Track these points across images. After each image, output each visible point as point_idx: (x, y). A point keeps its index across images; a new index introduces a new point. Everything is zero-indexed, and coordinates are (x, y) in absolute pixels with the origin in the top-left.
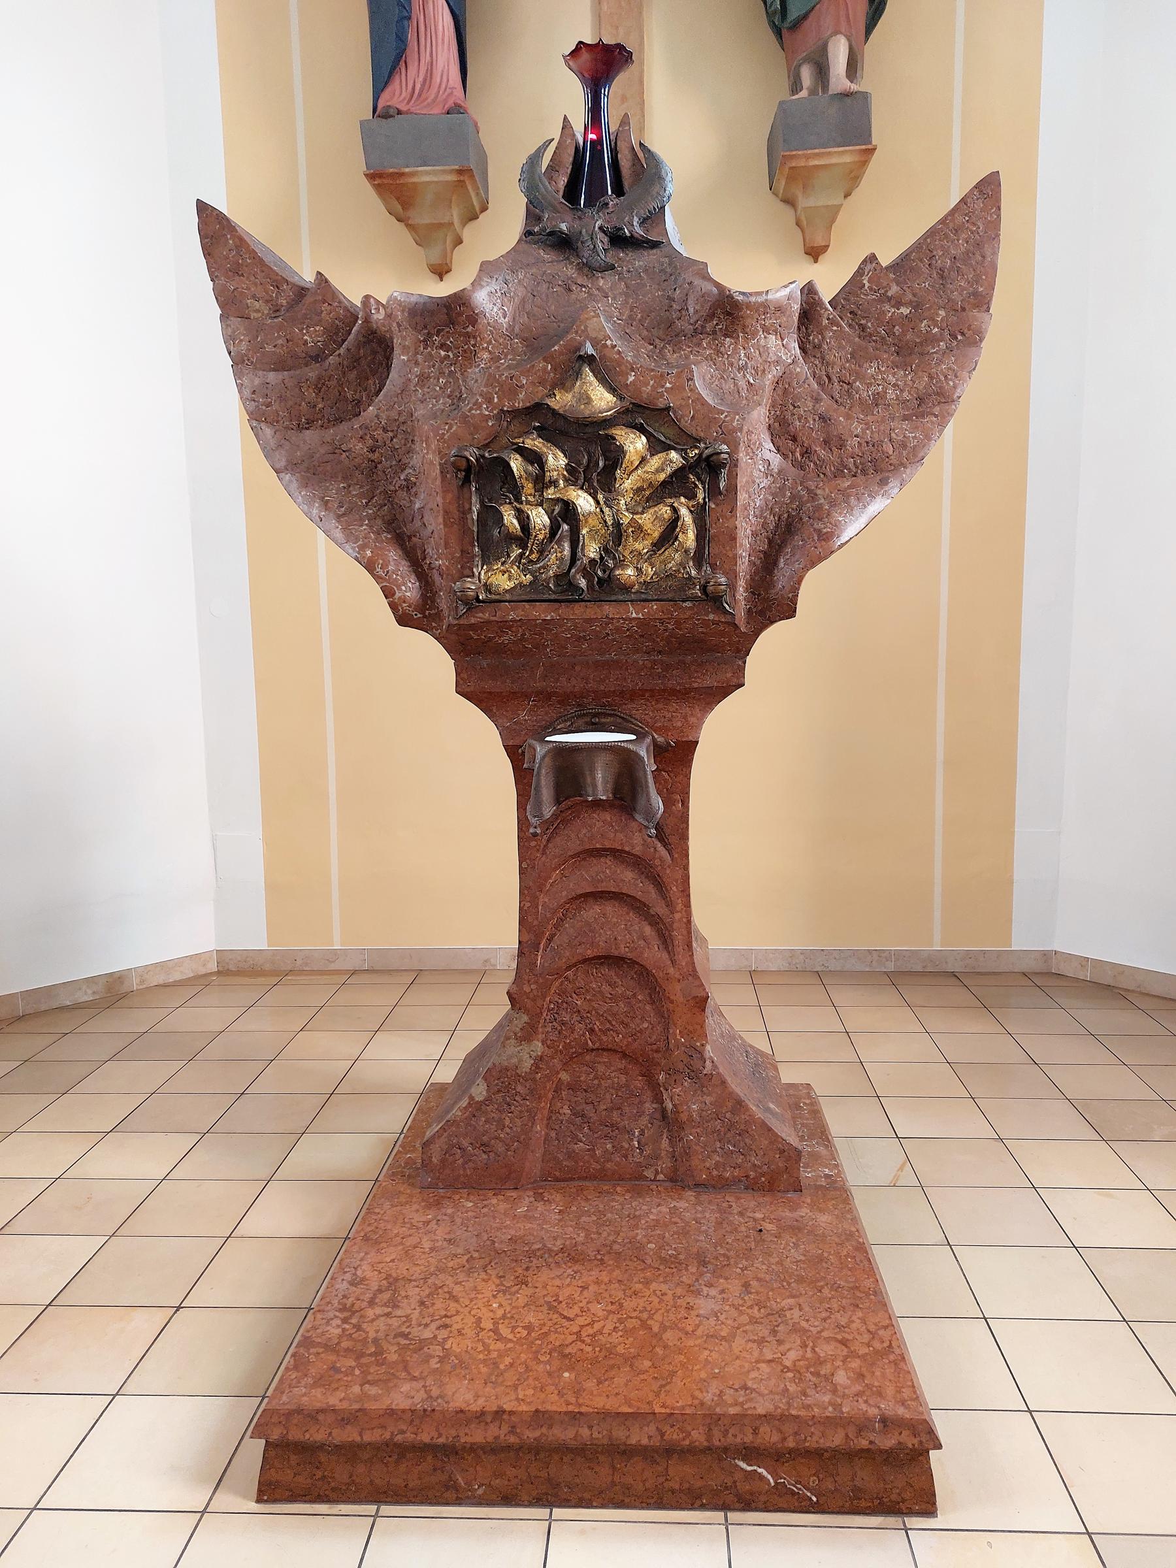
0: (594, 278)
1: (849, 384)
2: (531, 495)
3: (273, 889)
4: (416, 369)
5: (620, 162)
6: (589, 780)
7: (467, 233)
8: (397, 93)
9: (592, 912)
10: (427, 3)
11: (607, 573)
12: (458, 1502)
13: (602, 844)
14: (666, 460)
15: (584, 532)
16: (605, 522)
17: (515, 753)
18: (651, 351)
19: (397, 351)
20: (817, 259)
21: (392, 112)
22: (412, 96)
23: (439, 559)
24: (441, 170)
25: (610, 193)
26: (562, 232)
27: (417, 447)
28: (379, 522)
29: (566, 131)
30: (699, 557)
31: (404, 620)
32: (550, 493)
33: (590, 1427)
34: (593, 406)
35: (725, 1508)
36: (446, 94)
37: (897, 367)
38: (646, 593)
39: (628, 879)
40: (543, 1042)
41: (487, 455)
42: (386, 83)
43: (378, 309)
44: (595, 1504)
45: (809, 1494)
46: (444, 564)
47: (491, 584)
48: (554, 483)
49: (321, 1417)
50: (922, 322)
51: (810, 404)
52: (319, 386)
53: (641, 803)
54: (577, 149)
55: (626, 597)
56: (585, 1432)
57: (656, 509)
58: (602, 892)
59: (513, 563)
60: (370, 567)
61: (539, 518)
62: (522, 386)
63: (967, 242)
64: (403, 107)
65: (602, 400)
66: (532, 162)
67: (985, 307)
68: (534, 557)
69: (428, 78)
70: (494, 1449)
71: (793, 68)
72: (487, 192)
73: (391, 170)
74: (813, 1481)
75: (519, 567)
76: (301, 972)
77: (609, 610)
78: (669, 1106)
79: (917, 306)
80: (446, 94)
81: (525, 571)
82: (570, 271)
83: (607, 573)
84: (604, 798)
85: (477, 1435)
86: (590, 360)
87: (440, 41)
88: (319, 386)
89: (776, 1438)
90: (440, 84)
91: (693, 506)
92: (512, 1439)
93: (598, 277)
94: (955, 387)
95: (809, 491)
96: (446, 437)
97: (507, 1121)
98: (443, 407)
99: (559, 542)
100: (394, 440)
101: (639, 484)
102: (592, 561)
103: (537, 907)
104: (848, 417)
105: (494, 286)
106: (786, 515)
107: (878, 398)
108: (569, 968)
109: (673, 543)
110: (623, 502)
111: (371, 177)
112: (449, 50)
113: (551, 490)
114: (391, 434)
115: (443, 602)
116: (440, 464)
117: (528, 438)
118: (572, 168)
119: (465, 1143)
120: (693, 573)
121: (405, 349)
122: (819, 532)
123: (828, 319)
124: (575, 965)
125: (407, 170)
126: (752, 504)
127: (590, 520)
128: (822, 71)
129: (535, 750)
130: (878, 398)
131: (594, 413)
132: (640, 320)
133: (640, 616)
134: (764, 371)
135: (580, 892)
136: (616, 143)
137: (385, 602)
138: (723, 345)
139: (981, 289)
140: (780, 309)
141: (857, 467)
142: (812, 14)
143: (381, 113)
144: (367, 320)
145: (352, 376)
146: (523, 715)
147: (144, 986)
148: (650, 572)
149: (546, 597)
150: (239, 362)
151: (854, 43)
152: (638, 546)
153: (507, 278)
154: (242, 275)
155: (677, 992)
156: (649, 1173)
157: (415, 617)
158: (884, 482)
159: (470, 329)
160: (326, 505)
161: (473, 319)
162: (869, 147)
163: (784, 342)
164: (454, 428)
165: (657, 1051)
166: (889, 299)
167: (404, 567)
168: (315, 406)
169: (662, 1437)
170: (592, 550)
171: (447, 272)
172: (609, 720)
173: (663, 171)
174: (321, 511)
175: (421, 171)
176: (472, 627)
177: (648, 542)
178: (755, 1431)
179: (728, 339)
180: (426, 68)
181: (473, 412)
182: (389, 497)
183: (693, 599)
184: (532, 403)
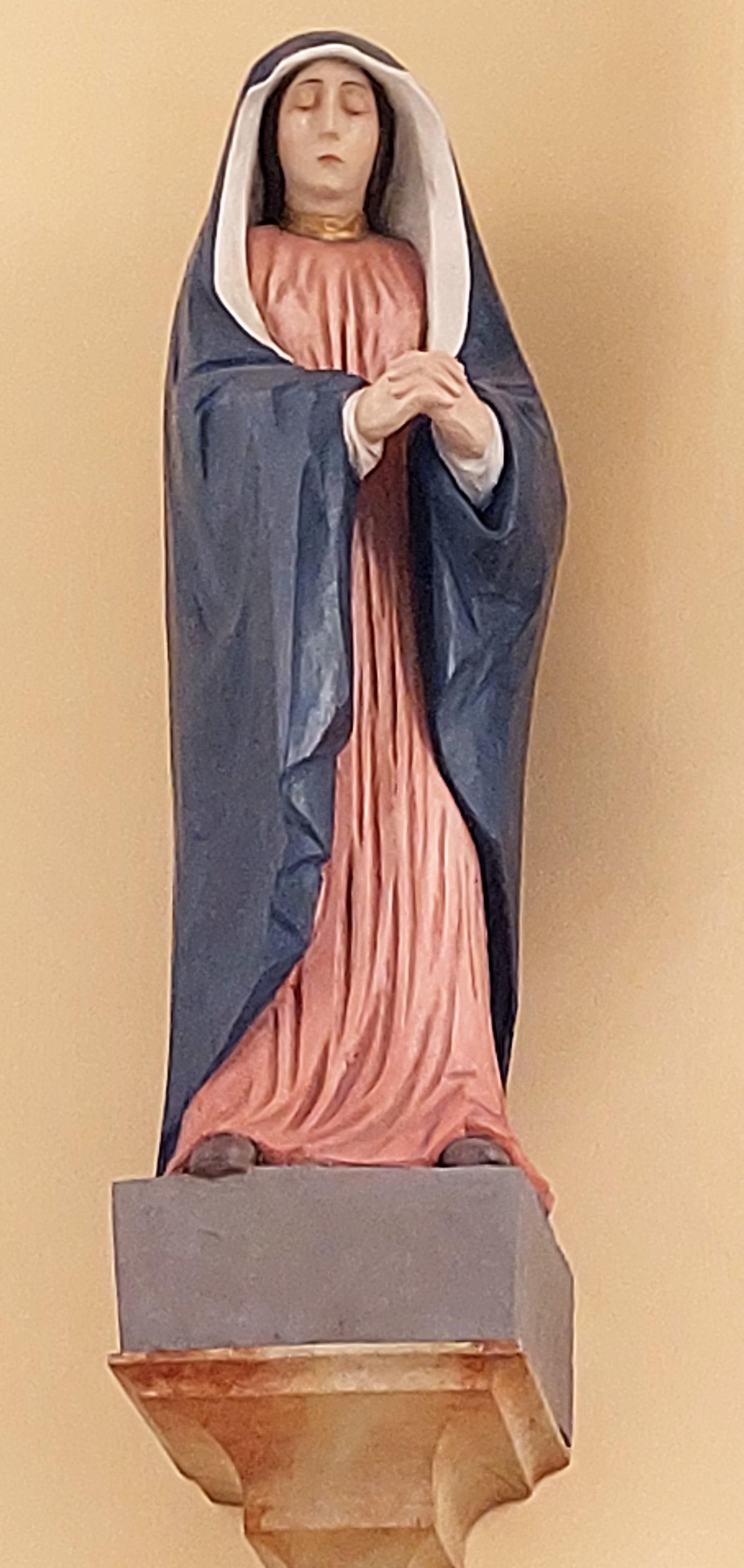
8: (259, 1092)
10: (391, 808)
13: (479, 1331)
21: (234, 1155)
24: (406, 1356)
73: (216, 1353)
90: (418, 1065)
112: (458, 950)
125: (274, 1353)
175: (327, 1358)
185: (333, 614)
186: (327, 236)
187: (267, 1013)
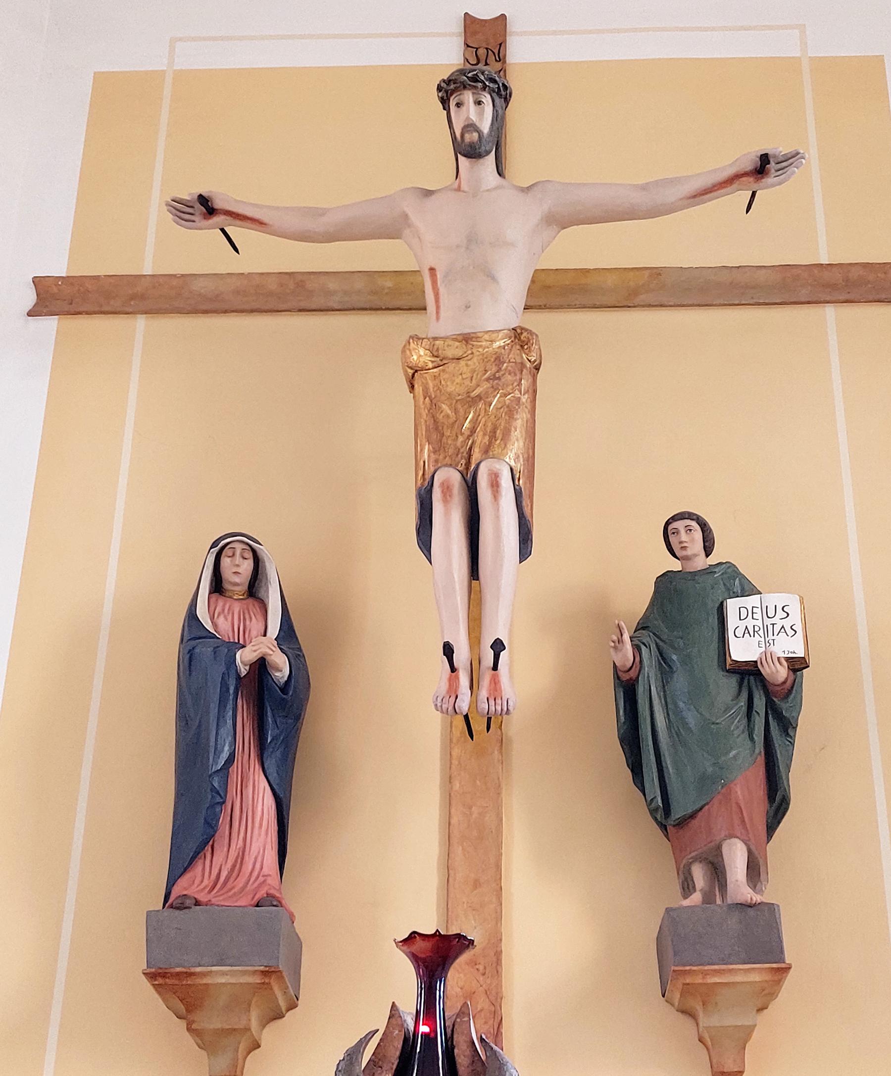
5: (457, 1058)
7: (269, 1036)
8: (197, 882)
21: (188, 902)
24: (241, 971)
29: (393, 1021)
42: (185, 870)
54: (406, 1039)
64: (202, 897)
69: (238, 866)
71: (682, 866)
72: (297, 987)
73: (178, 970)
87: (257, 825)
111: (151, 976)
118: (399, 1063)
125: (198, 969)
136: (453, 1031)
142: (700, 813)
151: (753, 848)
162: (783, 965)
180: (236, 855)
185: (230, 722)
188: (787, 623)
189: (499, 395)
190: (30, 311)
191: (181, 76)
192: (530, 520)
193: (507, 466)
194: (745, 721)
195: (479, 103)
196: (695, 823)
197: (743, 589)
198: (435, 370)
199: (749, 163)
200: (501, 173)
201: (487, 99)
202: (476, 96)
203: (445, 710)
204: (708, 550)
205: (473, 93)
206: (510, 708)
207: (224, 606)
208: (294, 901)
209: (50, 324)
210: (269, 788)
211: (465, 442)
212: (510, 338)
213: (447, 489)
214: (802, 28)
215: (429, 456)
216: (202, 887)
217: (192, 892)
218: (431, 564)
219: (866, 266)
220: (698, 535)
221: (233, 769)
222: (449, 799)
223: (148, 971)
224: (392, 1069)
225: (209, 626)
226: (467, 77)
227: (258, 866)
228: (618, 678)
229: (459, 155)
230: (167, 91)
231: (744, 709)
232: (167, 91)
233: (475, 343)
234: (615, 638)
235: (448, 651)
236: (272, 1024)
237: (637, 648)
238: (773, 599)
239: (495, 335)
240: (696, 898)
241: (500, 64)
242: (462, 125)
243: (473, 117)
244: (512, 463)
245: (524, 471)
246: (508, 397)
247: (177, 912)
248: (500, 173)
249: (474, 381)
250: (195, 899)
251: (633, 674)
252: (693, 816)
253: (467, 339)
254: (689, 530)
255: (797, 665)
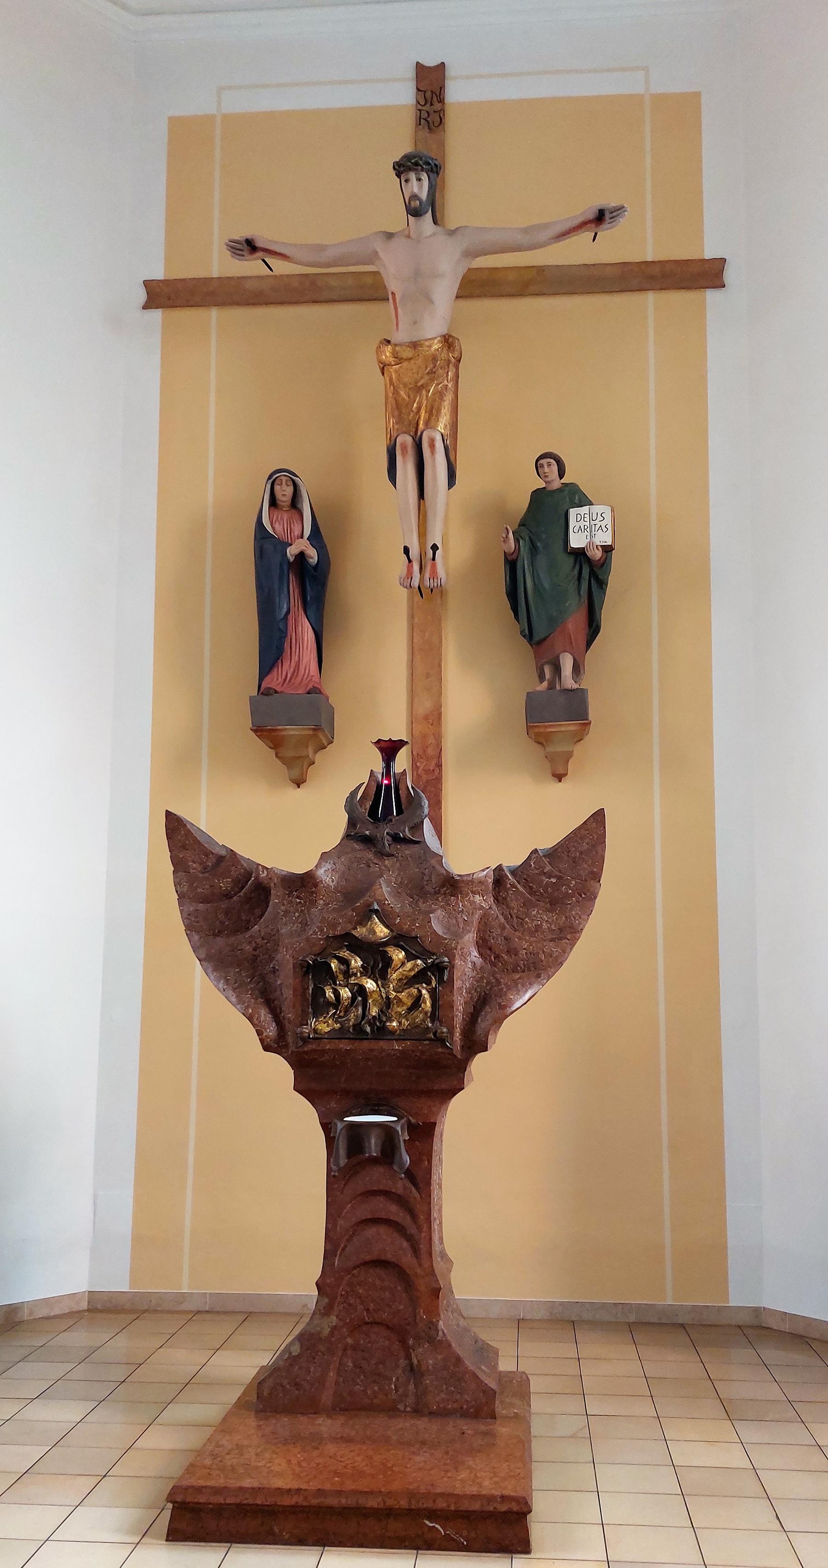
0: (383, 860)
1: (522, 919)
2: (342, 981)
3: (138, 1240)
4: (282, 908)
6: (367, 1144)
7: (319, 757)
8: (275, 680)
9: (371, 1232)
10: (298, 626)
11: (382, 1024)
12: (275, 1543)
14: (414, 965)
15: (370, 1001)
16: (382, 996)
17: (326, 1127)
18: (412, 902)
19: (272, 897)
20: (561, 780)
22: (285, 680)
23: (289, 1014)
25: (395, 814)
26: (367, 835)
27: (280, 948)
28: (257, 992)
30: (433, 1016)
31: (267, 1048)
32: (352, 980)
33: (346, 1498)
34: (376, 936)
35: (418, 1548)
36: (308, 680)
37: (548, 911)
38: (403, 1035)
39: (393, 1211)
40: (337, 1317)
41: (319, 959)
43: (263, 872)
44: (348, 1545)
45: (462, 1540)
46: (292, 1016)
47: (317, 1029)
48: (355, 975)
49: (204, 1490)
50: (562, 887)
51: (499, 931)
52: (227, 913)
53: (397, 1158)
55: (392, 1037)
56: (343, 1501)
57: (409, 990)
58: (378, 1218)
59: (330, 1017)
60: (250, 1018)
61: (345, 993)
62: (340, 923)
63: (587, 844)
65: (382, 931)
66: (352, 797)
67: (598, 879)
68: (342, 1014)
70: (295, 1510)
74: (465, 1533)
75: (333, 1020)
76: (155, 1311)
77: (382, 1044)
78: (415, 1362)
79: (559, 878)
80: (308, 680)
81: (336, 1022)
82: (371, 856)
83: (382, 1024)
84: (375, 1155)
85: (288, 1501)
86: (376, 912)
87: (305, 647)
88: (227, 913)
89: (444, 1505)
91: (429, 989)
92: (305, 1504)
93: (385, 860)
94: (580, 924)
95: (497, 980)
96: (297, 949)
97: (312, 1369)
98: (296, 929)
99: (356, 1007)
100: (268, 944)
101: (400, 977)
102: (374, 1017)
103: (336, 1227)
104: (520, 938)
105: (328, 866)
106: (483, 993)
107: (538, 928)
108: (355, 1268)
109: (418, 1009)
110: (391, 986)
113: (353, 978)
114: (265, 941)
115: (290, 1039)
116: (293, 963)
117: (341, 951)
119: (285, 1382)
120: (430, 1025)
121: (277, 897)
122: (500, 1004)
123: (510, 884)
124: (358, 1266)
125: (280, 727)
126: (465, 986)
127: (373, 995)
128: (557, 669)
129: (337, 1125)
130: (538, 928)
131: (377, 939)
132: (406, 884)
133: (400, 1048)
134: (473, 913)
135: (364, 1218)
137: (258, 1038)
138: (450, 900)
139: (595, 870)
140: (481, 882)
141: (525, 966)
143: (264, 692)
144: (257, 878)
145: (247, 907)
146: (333, 1105)
147: (32, 1317)
148: (407, 1023)
149: (347, 1036)
150: (181, 897)
151: (576, 657)
152: (399, 1009)
153: (335, 861)
154: (188, 849)
155: (422, 1285)
156: (401, 1407)
157: (274, 1047)
158: (539, 976)
159: (314, 889)
160: (227, 981)
161: (316, 885)
163: (484, 898)
164: (302, 944)
165: (408, 1324)
166: (545, 874)
167: (269, 1017)
168: (224, 923)
169: (384, 1504)
170: (374, 1011)
171: (303, 783)
172: (384, 1108)
173: (423, 802)
174: (224, 985)
176: (305, 1052)
177: (405, 1008)
178: (434, 1501)
179: (452, 897)
181: (313, 936)
182: (263, 977)
183: (430, 1039)
184: (345, 932)
185: (286, 590)
186: (284, 509)
187: (276, 665)
188: (603, 524)
189: (434, 385)
190: (144, 306)
191: (225, 116)
192: (454, 464)
193: (439, 432)
194: (577, 583)
195: (419, 180)
196: (546, 643)
197: (580, 501)
198: (397, 366)
199: (591, 215)
200: (436, 222)
201: (424, 176)
202: (417, 175)
203: (405, 586)
204: (561, 475)
205: (416, 174)
206: (442, 584)
207: (278, 516)
208: (327, 689)
209: (157, 315)
210: (311, 627)
211: (414, 418)
212: (442, 343)
213: (404, 448)
214: (646, 69)
215: (393, 426)
216: (278, 683)
217: (273, 686)
218: (396, 488)
219: (676, 262)
220: (555, 468)
221: (290, 616)
222: (412, 628)
223: (253, 728)
224: (371, 800)
225: (271, 532)
226: (411, 163)
227: (307, 671)
228: (507, 558)
229: (409, 215)
230: (218, 132)
231: (576, 576)
232: (218, 132)
233: (420, 348)
234: (504, 536)
235: (406, 550)
236: (321, 750)
237: (517, 540)
238: (597, 509)
239: (431, 342)
240: (545, 684)
241: (440, 104)
242: (409, 195)
243: (416, 190)
244: (443, 431)
245: (450, 435)
246: (440, 386)
247: (266, 697)
248: (435, 222)
249: (420, 375)
250: (274, 689)
251: (514, 557)
252: (544, 639)
253: (415, 345)
254: (549, 465)
255: (607, 550)
